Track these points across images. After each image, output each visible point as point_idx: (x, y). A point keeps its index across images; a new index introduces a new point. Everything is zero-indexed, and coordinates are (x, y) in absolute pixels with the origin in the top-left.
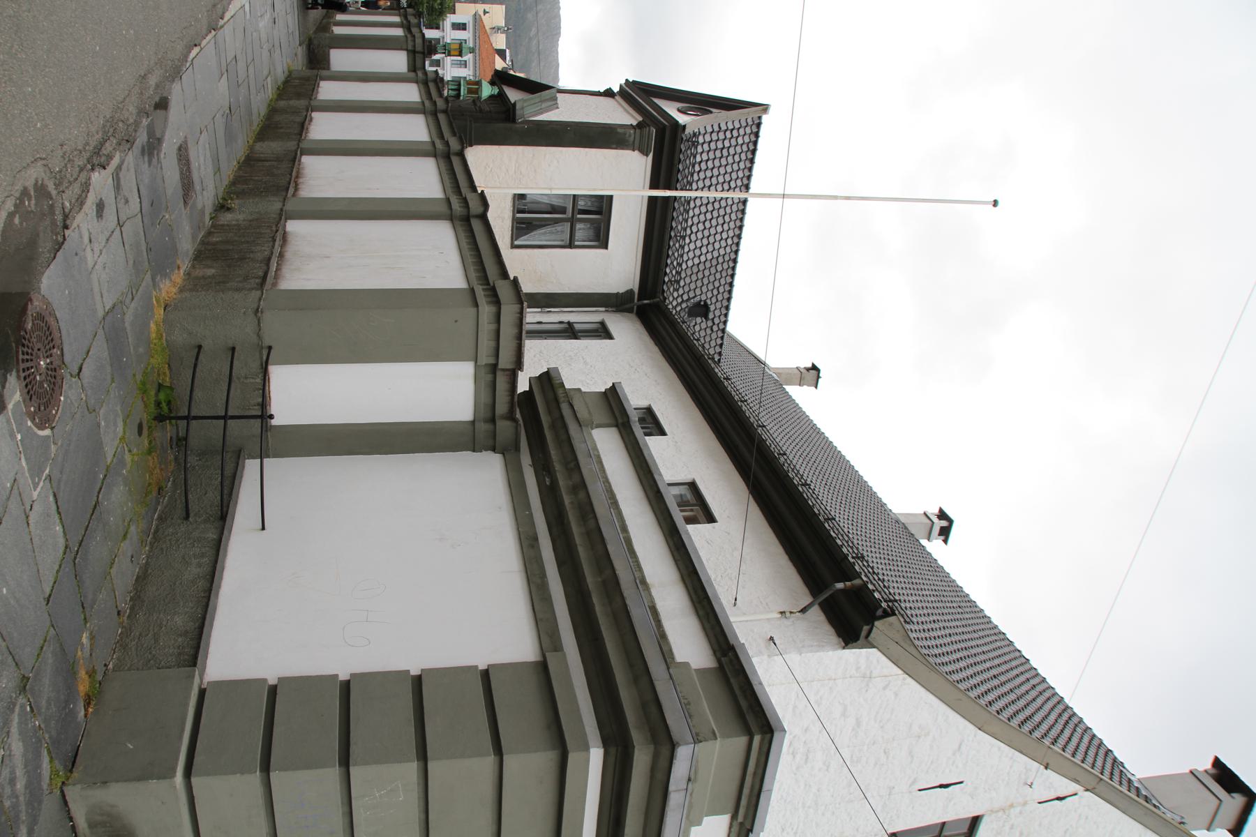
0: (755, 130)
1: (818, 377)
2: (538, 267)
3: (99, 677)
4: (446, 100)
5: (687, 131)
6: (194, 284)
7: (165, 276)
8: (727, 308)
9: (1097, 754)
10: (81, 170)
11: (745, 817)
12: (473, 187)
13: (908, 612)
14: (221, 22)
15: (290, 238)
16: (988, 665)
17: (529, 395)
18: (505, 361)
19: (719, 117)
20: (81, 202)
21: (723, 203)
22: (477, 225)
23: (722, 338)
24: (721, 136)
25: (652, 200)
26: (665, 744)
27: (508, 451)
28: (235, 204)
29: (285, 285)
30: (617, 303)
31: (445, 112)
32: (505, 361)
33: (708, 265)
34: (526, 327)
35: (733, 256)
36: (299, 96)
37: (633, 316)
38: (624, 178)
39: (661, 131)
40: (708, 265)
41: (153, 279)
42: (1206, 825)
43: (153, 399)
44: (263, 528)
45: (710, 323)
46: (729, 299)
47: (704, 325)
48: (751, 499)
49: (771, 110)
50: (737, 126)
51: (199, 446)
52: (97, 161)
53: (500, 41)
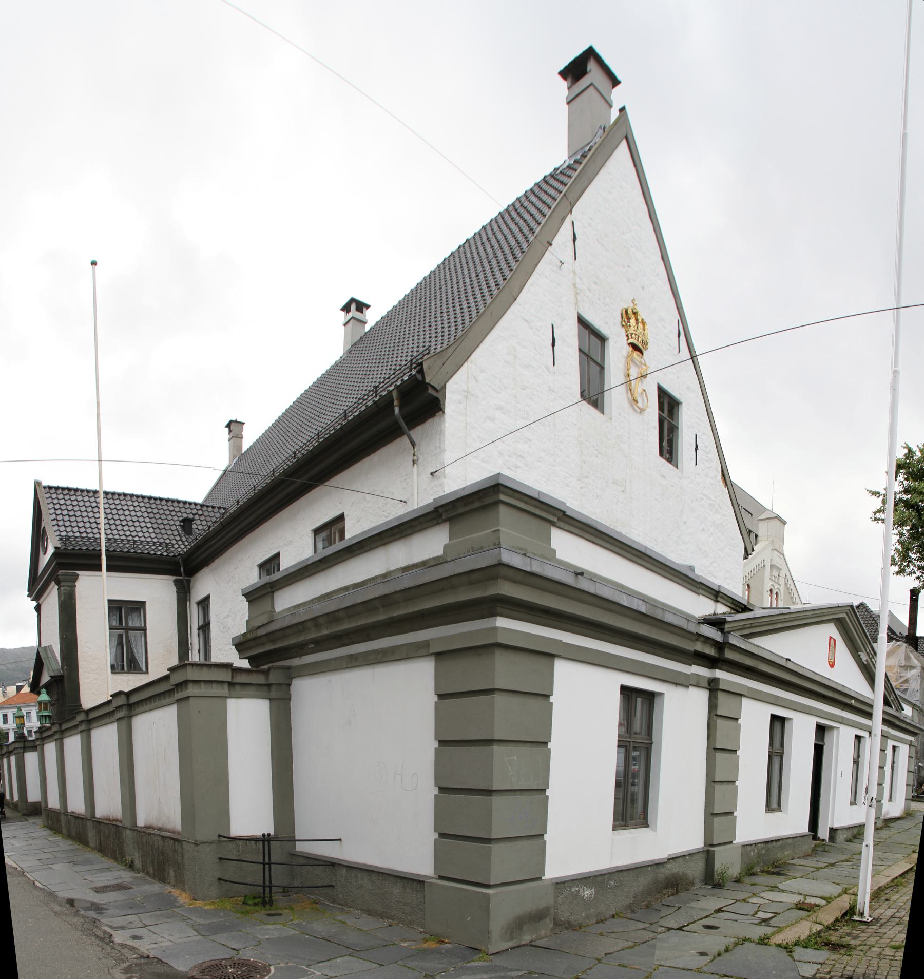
0: (53, 491)
1: (236, 421)
2: (160, 655)
3: (428, 936)
4: (53, 724)
5: (59, 546)
6: (180, 883)
7: (175, 900)
8: (185, 503)
9: (546, 192)
10: (113, 948)
11: (555, 515)
12: (108, 703)
13: (421, 349)
14: (19, 869)
15: (148, 824)
16: (467, 280)
17: (251, 659)
18: (226, 676)
19: (47, 522)
20: (132, 949)
21: (108, 511)
22: (134, 699)
23: (208, 506)
24: (60, 517)
25: (109, 569)
26: (499, 571)
27: (290, 674)
28: (129, 859)
29: (179, 827)
30: (183, 592)
31: (60, 725)
32: (226, 676)
33: (153, 521)
34: (202, 661)
35: (146, 500)
36: (59, 821)
37: (193, 580)
38: (96, 590)
39: (61, 566)
40: (153, 521)
41: (178, 907)
42: (608, 107)
43: (252, 908)
44: (340, 840)
45: (197, 517)
46: (178, 502)
47: (198, 522)
48: (327, 483)
49: (38, 479)
50: (52, 505)
51: (280, 877)
52: (107, 939)
53: (12, 690)
